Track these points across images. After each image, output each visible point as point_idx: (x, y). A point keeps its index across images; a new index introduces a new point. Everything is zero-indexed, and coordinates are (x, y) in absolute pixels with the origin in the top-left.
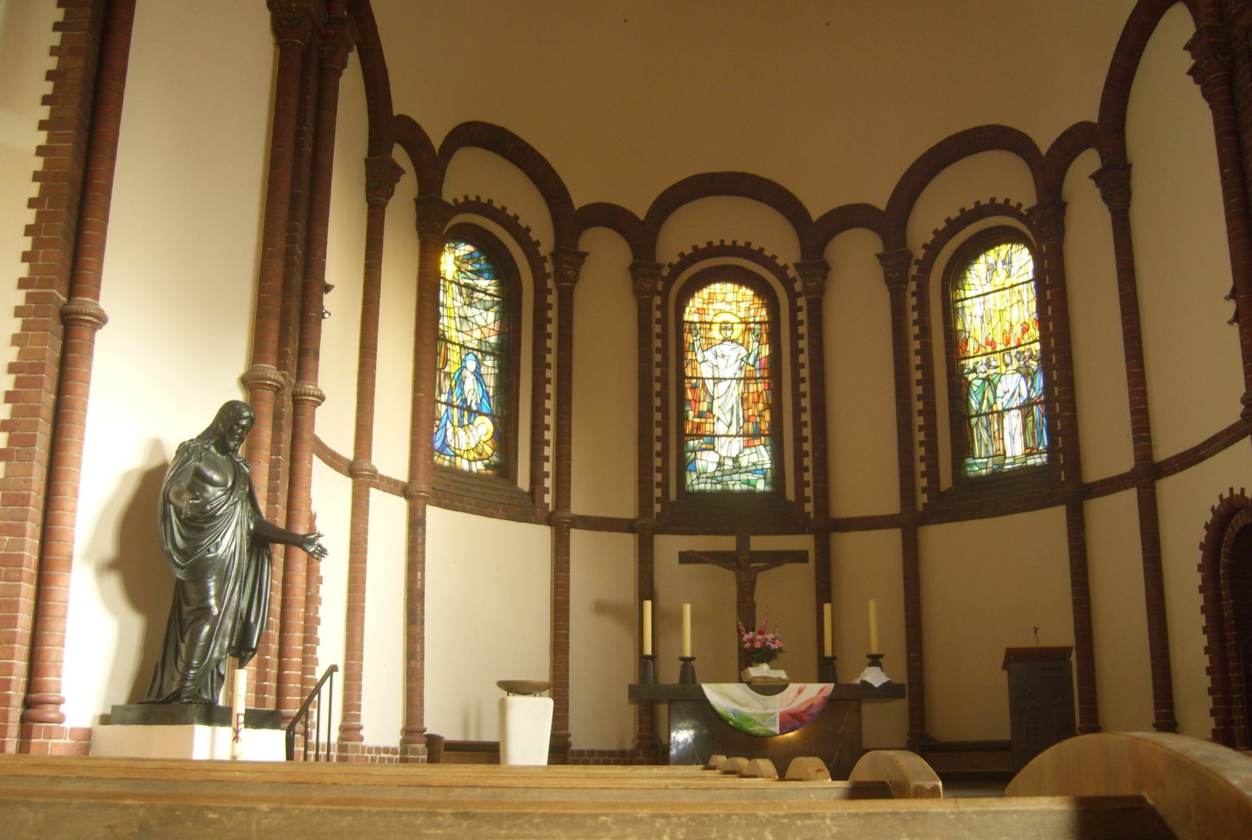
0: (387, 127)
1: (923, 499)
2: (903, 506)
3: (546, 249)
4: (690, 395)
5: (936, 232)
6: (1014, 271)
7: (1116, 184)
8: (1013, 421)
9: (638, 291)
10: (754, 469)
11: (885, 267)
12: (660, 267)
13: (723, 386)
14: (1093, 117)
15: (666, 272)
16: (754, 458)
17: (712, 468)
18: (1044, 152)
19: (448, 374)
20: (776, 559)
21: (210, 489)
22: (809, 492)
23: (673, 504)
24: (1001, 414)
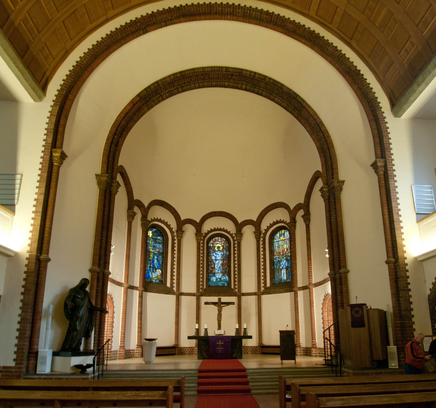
0: (133, 203)
1: (262, 289)
2: (258, 290)
3: (175, 229)
4: (210, 263)
5: (267, 227)
6: (285, 236)
7: (307, 218)
8: (284, 271)
9: (197, 240)
10: (225, 281)
11: (255, 235)
12: (202, 234)
13: (217, 262)
14: (303, 202)
15: (204, 235)
16: (225, 278)
17: (214, 280)
18: (292, 209)
19: (150, 260)
20: (228, 304)
21: (78, 299)
22: (237, 287)
23: (205, 290)
24: (281, 270)
